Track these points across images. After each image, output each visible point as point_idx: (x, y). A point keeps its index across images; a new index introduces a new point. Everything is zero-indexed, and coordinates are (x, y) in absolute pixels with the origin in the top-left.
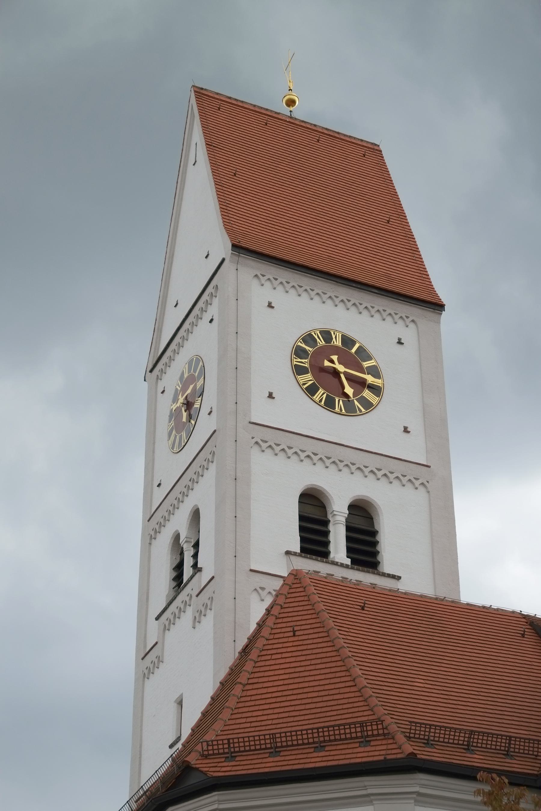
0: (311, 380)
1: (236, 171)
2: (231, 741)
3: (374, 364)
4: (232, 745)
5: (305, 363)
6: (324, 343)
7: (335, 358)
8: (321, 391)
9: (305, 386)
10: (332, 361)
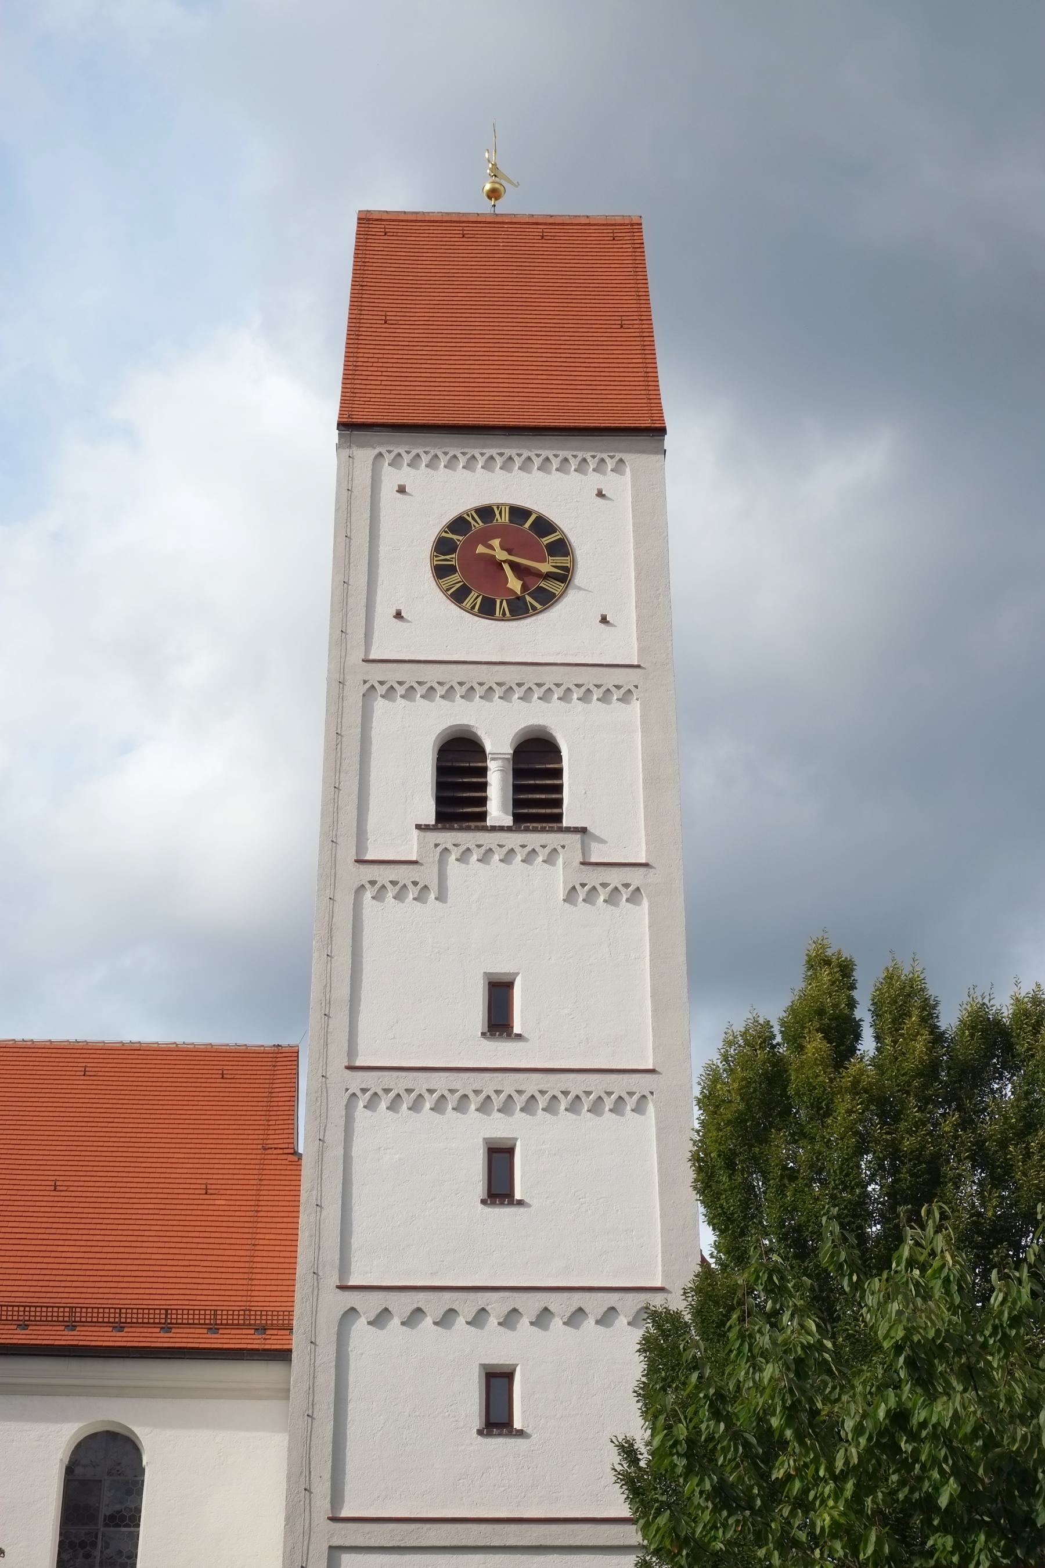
0: (459, 582)
1: (622, 320)
2: (169, 1312)
3: (560, 536)
4: (169, 1316)
5: (453, 559)
6: (481, 523)
7: (496, 543)
8: (474, 594)
9: (450, 592)
10: (492, 548)
